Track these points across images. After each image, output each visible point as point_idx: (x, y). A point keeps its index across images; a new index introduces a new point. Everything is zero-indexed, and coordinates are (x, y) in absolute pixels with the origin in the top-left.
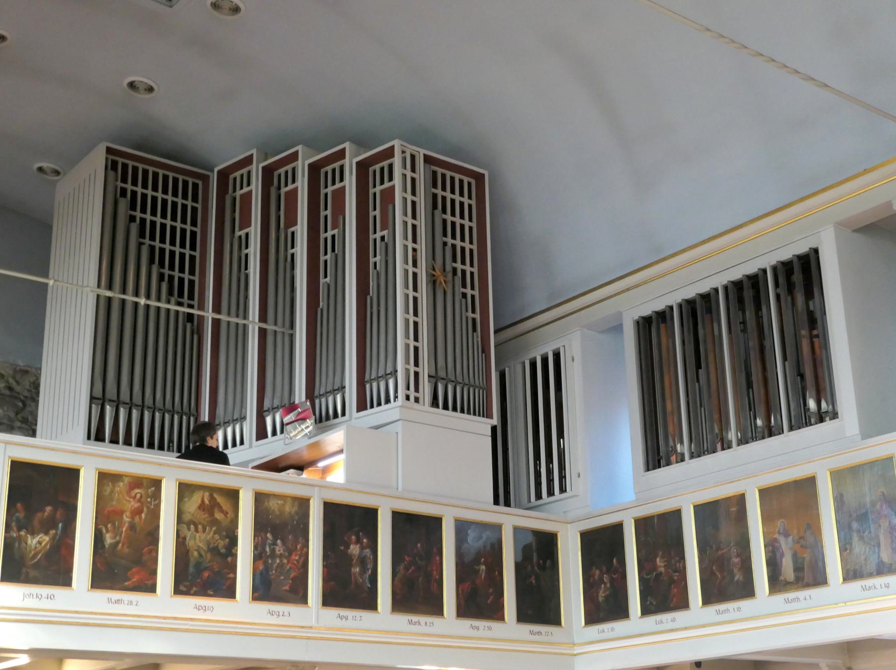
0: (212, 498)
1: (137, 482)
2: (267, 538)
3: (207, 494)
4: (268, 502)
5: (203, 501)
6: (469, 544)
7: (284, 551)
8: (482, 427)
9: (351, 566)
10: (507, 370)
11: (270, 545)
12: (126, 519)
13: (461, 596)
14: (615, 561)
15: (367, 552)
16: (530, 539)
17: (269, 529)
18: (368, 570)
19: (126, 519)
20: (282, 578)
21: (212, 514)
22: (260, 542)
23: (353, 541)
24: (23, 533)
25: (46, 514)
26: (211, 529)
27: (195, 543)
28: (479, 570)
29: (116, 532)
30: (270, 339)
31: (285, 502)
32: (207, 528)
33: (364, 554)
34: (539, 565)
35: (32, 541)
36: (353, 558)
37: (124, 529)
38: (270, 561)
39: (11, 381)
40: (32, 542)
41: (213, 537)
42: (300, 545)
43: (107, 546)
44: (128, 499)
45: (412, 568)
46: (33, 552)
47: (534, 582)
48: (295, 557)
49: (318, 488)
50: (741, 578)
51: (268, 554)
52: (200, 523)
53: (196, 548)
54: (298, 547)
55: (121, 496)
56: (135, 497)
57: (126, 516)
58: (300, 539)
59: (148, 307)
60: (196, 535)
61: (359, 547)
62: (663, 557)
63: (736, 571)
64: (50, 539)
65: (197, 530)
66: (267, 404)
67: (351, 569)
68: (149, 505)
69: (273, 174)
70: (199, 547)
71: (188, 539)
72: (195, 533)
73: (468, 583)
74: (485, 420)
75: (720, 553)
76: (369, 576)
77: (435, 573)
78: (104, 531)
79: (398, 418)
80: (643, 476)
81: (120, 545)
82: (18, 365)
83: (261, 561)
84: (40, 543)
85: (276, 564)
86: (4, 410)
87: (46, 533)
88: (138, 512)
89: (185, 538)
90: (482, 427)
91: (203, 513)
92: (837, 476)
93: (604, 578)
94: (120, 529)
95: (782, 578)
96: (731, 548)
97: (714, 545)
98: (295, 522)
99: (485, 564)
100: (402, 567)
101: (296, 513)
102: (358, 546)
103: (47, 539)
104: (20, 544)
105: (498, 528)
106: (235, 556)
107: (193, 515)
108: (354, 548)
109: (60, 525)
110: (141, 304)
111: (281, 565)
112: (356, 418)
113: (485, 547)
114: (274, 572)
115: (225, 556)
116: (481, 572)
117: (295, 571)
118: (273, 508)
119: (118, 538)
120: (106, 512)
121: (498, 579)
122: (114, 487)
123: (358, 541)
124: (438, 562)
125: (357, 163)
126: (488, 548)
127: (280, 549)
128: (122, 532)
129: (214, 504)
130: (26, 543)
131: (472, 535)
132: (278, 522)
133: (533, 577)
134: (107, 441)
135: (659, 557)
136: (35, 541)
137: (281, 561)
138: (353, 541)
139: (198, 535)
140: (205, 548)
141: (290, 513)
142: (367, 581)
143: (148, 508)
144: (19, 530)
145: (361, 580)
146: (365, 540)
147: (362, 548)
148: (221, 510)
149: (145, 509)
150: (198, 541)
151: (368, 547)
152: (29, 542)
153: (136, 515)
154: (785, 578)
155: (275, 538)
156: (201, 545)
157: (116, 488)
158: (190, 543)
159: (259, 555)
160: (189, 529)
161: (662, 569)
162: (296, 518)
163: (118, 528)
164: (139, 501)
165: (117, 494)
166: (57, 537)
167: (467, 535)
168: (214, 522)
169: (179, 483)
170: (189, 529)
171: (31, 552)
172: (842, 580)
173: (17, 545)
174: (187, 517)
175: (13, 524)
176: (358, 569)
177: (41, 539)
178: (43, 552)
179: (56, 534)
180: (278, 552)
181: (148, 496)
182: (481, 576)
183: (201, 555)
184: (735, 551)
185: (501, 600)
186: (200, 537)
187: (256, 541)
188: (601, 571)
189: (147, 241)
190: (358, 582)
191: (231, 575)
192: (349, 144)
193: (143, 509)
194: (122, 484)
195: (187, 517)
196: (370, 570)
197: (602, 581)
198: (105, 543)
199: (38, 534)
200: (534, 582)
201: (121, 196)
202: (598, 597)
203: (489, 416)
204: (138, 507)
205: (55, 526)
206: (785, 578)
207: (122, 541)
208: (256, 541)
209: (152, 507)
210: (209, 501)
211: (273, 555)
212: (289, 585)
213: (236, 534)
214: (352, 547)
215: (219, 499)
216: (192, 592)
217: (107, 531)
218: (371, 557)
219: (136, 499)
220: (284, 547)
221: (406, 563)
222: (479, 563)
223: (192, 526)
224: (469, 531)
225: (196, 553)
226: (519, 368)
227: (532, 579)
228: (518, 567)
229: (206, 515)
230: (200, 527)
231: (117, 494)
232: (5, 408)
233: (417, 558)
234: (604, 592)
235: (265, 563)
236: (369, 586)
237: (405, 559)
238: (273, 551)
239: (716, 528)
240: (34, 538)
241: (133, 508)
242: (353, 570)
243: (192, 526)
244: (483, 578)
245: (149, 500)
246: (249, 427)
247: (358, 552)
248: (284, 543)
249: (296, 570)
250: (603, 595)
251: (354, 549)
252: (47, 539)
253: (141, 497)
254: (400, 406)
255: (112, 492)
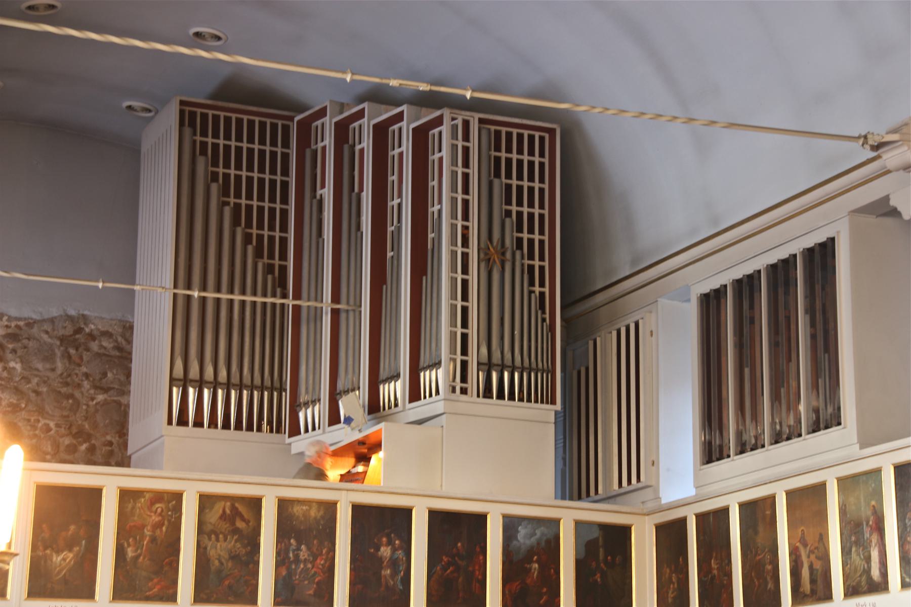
0: (233, 508)
1: (159, 496)
2: (290, 544)
3: (228, 504)
4: (292, 509)
5: (224, 511)
6: (518, 541)
7: (308, 556)
8: (547, 413)
9: (381, 568)
10: (598, 340)
11: (294, 551)
12: (148, 532)
13: (507, 596)
14: (681, 559)
15: (400, 554)
16: (596, 533)
17: (293, 535)
18: (401, 572)
19: (148, 532)
20: (306, 582)
21: (233, 523)
22: (283, 548)
23: (384, 543)
24: (48, 552)
25: (70, 532)
26: (233, 538)
27: (216, 553)
28: (530, 569)
29: (138, 545)
30: (343, 316)
31: (310, 507)
32: (229, 537)
33: (396, 556)
34: (606, 562)
35: (57, 559)
36: (384, 560)
37: (145, 543)
38: (293, 567)
39: (120, 339)
40: (57, 559)
41: (234, 546)
42: (326, 549)
43: (128, 560)
44: (149, 513)
45: (451, 568)
46: (58, 569)
47: (599, 580)
48: (320, 562)
49: (346, 492)
50: (772, 588)
51: (291, 560)
52: (221, 533)
53: (217, 557)
54: (324, 551)
55: (142, 511)
56: (156, 512)
57: (147, 530)
58: (326, 543)
59: (203, 300)
60: (217, 545)
61: (391, 549)
62: (716, 559)
63: (768, 578)
64: (74, 556)
65: (217, 540)
66: (340, 386)
67: (381, 572)
68: (170, 518)
69: (349, 128)
70: (219, 555)
71: (209, 548)
72: (216, 542)
73: (518, 583)
74: (549, 406)
75: (758, 558)
76: (401, 578)
77: (477, 573)
78: (126, 545)
79: (442, 411)
80: (700, 470)
81: (141, 558)
82: (127, 322)
83: (284, 567)
84: (64, 559)
85: (300, 570)
86: (113, 373)
87: (70, 550)
88: (159, 525)
89: (205, 548)
90: (547, 413)
91: (224, 523)
92: (843, 482)
93: (673, 578)
94: (142, 543)
95: (802, 590)
96: (765, 554)
97: (753, 550)
98: (321, 527)
99: (537, 561)
100: (438, 568)
101: (322, 517)
102: (390, 548)
103: (71, 555)
104: (45, 562)
105: (555, 523)
106: (257, 563)
107: (214, 525)
108: (385, 551)
109: (84, 542)
110: (195, 297)
111: (306, 570)
112: (410, 409)
113: (538, 544)
114: (297, 577)
115: (247, 564)
116: (533, 571)
117: (321, 576)
118: (297, 514)
119: (139, 551)
120: (128, 527)
121: (554, 577)
122: (135, 504)
123: (390, 543)
124: (481, 561)
125: (414, 129)
126: (543, 544)
127: (304, 554)
128: (143, 545)
129: (236, 513)
130: (51, 560)
131: (522, 532)
132: (302, 528)
133: (598, 575)
134: (191, 423)
135: (714, 558)
136: (59, 558)
137: (305, 566)
138: (384, 543)
139: (219, 545)
140: (227, 556)
141: (315, 518)
142: (399, 583)
143: (169, 521)
144: (46, 548)
145: (392, 583)
146: (397, 542)
147: (394, 550)
148: (243, 519)
149: (166, 522)
150: (220, 549)
151: (401, 548)
152: (54, 559)
153: (157, 528)
154: (804, 590)
155: (299, 543)
156: (222, 553)
157: (137, 504)
158: (212, 553)
159: (282, 560)
160: (210, 539)
161: (715, 572)
162: (322, 522)
163: (139, 543)
164: (160, 515)
165: (138, 510)
166: (81, 554)
167: (518, 532)
168: (236, 531)
169: (199, 495)
170: (210, 539)
171: (56, 568)
172: (843, 596)
173: (43, 562)
174: (208, 528)
175: (39, 544)
176: (389, 572)
177: (65, 557)
178: (67, 568)
179: (80, 551)
180: (302, 558)
181: (169, 510)
182: (533, 575)
183: (222, 564)
184: (769, 557)
185: (556, 600)
186: (221, 546)
187: (279, 547)
188: (671, 570)
189: (232, 200)
190: (389, 584)
191: (254, 582)
192: (407, 108)
193: (164, 522)
194: (143, 500)
195: (208, 528)
196: (402, 573)
197: (671, 581)
198: (127, 557)
199: (62, 551)
200: (599, 580)
201: (201, 154)
202: (668, 597)
203: (553, 402)
204: (160, 521)
205: (79, 544)
206: (804, 590)
207: (143, 554)
208: (279, 547)
209: (173, 520)
210: (231, 511)
211: (297, 560)
212: (313, 589)
213: (258, 542)
214: (382, 549)
215: (241, 508)
216: (213, 599)
217: (129, 545)
218: (404, 558)
219: (157, 514)
220: (309, 553)
221: (443, 563)
222: (531, 561)
223: (213, 536)
224: (520, 528)
225: (217, 563)
226: (614, 333)
227: (596, 577)
228: (580, 565)
229: (228, 525)
230: (221, 536)
231: (138, 510)
232: (115, 372)
233: (456, 558)
234: (672, 593)
235: (288, 568)
236: (401, 588)
237: (442, 559)
238: (297, 557)
239: (756, 533)
240: (58, 556)
241: (154, 522)
242: (383, 572)
243: (213, 536)
244: (535, 577)
245: (170, 513)
246: (317, 412)
247: (389, 554)
248: (309, 549)
249: (322, 574)
250: (672, 596)
251: (385, 552)
252: (71, 555)
253: (162, 511)
254: (444, 399)
255: (133, 508)
